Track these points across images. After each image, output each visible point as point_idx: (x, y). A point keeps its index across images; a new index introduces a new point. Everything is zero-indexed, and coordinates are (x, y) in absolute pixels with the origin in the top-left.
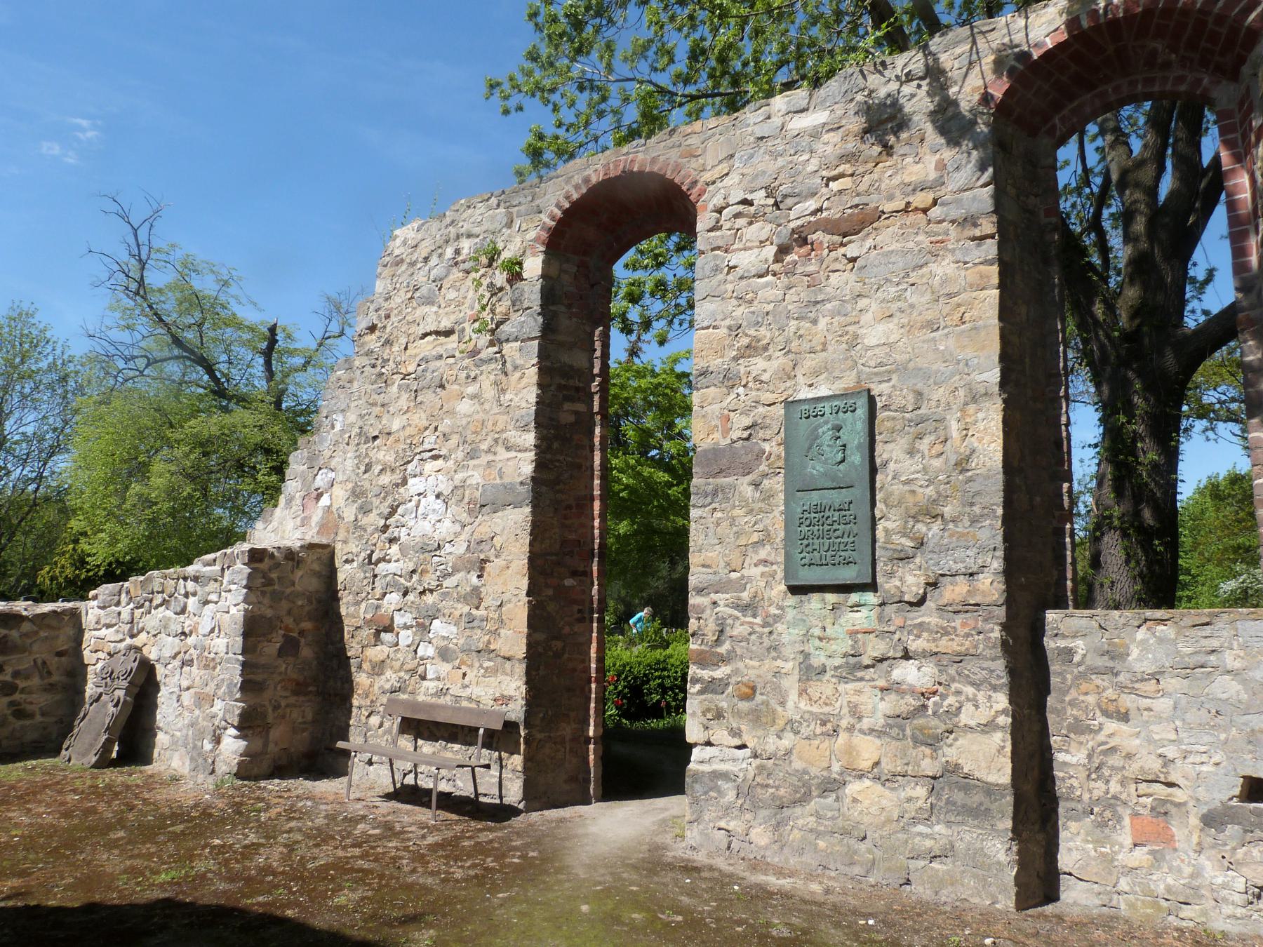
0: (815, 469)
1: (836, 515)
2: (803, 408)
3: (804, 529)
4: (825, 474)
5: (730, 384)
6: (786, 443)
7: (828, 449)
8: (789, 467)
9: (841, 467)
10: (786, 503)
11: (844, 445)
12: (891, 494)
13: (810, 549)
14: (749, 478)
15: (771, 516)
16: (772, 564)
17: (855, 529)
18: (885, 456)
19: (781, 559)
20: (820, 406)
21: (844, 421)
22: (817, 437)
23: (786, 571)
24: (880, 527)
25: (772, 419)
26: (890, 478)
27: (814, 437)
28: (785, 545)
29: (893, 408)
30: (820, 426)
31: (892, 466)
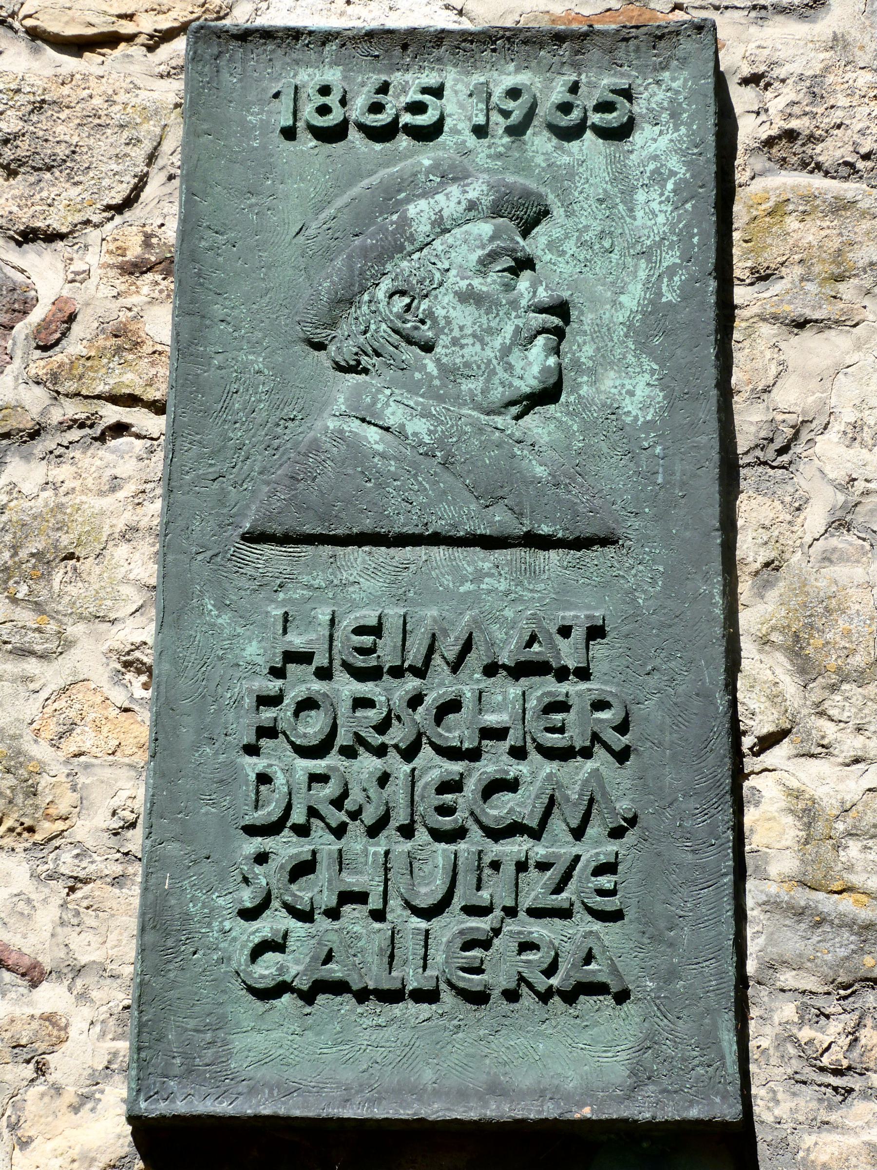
0: (375, 423)
1: (505, 702)
2: (309, 77)
3: (288, 769)
4: (443, 457)
6: (186, 268)
7: (464, 317)
8: (193, 400)
9: (538, 425)
10: (172, 600)
11: (561, 309)
12: (831, 607)
13: (317, 891)
15: (51, 675)
16: (34, 976)
17: (622, 791)
18: (790, 398)
19: (113, 937)
20: (410, 83)
21: (563, 179)
22: (398, 245)
24: (771, 785)
25: (94, 122)
26: (815, 519)
27: (379, 242)
29: (830, 152)
31: (830, 453)
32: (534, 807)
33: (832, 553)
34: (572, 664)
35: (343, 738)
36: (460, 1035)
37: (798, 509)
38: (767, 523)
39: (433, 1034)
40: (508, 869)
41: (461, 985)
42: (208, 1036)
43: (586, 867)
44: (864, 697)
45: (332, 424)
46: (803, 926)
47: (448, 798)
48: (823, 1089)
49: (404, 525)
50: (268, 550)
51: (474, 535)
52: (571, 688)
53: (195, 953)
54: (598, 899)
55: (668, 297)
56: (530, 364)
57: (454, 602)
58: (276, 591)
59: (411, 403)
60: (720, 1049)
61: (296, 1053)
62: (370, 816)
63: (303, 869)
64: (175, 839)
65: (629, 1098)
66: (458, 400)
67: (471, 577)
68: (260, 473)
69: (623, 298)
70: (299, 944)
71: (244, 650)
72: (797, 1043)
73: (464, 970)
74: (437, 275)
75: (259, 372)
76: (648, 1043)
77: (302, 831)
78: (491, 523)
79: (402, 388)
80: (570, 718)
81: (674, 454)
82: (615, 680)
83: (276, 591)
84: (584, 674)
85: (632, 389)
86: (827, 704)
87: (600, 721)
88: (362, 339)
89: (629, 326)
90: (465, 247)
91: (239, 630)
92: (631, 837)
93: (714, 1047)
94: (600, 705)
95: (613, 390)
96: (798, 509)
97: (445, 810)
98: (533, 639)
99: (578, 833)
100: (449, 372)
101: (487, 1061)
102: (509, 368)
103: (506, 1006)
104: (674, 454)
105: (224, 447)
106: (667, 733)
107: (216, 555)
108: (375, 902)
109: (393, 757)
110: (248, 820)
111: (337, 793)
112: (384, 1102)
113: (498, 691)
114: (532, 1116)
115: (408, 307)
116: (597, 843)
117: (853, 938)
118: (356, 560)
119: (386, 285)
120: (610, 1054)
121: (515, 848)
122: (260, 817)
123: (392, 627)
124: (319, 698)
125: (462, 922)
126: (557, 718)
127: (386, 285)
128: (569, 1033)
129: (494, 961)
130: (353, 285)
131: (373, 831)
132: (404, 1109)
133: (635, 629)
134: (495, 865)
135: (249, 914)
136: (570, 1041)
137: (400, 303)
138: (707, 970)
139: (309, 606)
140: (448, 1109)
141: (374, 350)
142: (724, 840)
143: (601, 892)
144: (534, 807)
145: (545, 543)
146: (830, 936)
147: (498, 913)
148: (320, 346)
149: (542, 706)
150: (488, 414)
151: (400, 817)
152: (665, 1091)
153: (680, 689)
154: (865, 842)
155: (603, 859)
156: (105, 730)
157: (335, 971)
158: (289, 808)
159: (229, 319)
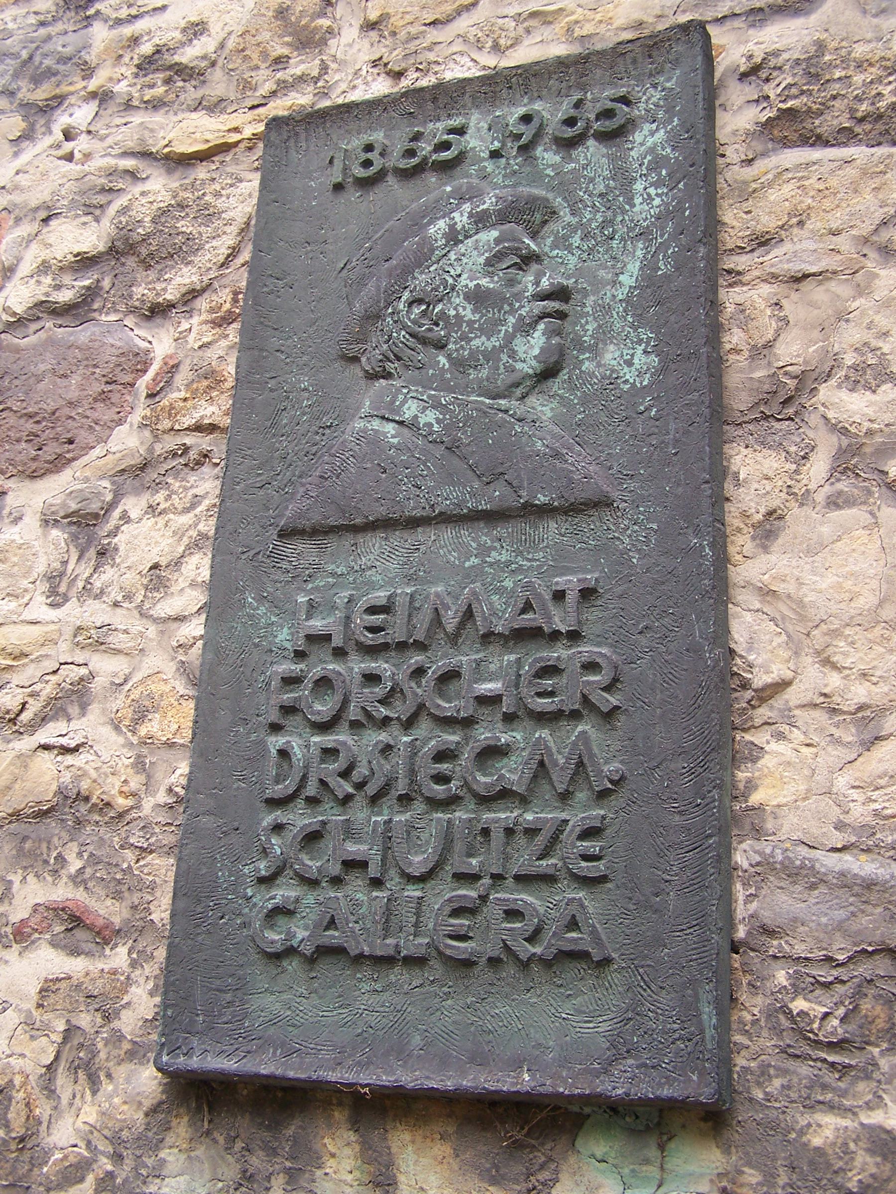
5: (41, 94)
11: (561, 294)
14: (55, 490)
18: (792, 351)
21: (565, 185)
22: (423, 257)
23: (174, 989)
28: (189, 832)
30: (433, 212)
32: (523, 773)
33: (837, 498)
34: (563, 629)
35: (353, 712)
36: (449, 1002)
37: (804, 458)
38: (771, 474)
39: (424, 1000)
40: (497, 836)
41: (448, 952)
42: (229, 997)
43: (572, 831)
44: (870, 641)
45: (359, 424)
46: (798, 888)
47: (444, 767)
48: (819, 1064)
49: (413, 509)
50: (301, 546)
51: (478, 511)
52: (559, 653)
53: (222, 918)
54: (584, 864)
55: (663, 268)
56: (532, 347)
57: (459, 577)
58: (306, 581)
59: (425, 397)
60: (700, 1022)
61: (301, 1014)
62: (371, 789)
63: (312, 838)
64: (209, 813)
65: (606, 1072)
66: (466, 389)
67: (475, 552)
68: (300, 477)
69: (621, 278)
70: (308, 910)
71: (276, 636)
72: (789, 1014)
73: (451, 937)
74: (450, 281)
75: (305, 389)
76: (631, 1015)
77: (312, 801)
78: (491, 499)
79: (417, 385)
80: (562, 681)
81: (668, 414)
82: (610, 641)
83: (306, 581)
84: (574, 636)
85: (628, 360)
86: (831, 650)
87: (589, 683)
88: (385, 347)
89: (627, 300)
90: (475, 253)
91: (273, 619)
92: (617, 801)
93: (694, 1020)
94: (591, 666)
95: (614, 363)
96: (804, 458)
97: (442, 779)
98: (527, 607)
99: (565, 797)
100: (460, 365)
101: (473, 1029)
102: (513, 354)
103: (489, 976)
104: (668, 414)
105: (272, 457)
106: (658, 692)
107: (258, 553)
108: (373, 871)
109: (395, 729)
110: (269, 794)
111: (345, 766)
112: (372, 1067)
113: (495, 660)
114: (505, 1089)
115: (424, 313)
116: (586, 807)
117: (851, 899)
118: (374, 546)
119: (406, 295)
120: (591, 1025)
121: (503, 815)
122: (279, 790)
123: (401, 603)
124: (332, 676)
125: (454, 890)
126: (548, 683)
127: (406, 295)
128: (552, 1001)
129: (483, 928)
130: (379, 302)
131: (374, 800)
132: (387, 1075)
133: (629, 588)
134: (486, 832)
135: (266, 881)
136: (553, 1011)
137: (417, 310)
138: (690, 937)
139: (332, 592)
140: (427, 1078)
141: (395, 355)
142: (709, 800)
143: (586, 858)
144: (523, 773)
145: (545, 511)
146: (828, 898)
147: (486, 881)
148: (355, 359)
149: (533, 671)
150: (494, 399)
151: (401, 787)
152: (645, 1065)
153: (672, 647)
154: (870, 794)
155: (589, 823)
156: (170, 714)
157: (335, 938)
158: (304, 778)
159: (283, 348)
